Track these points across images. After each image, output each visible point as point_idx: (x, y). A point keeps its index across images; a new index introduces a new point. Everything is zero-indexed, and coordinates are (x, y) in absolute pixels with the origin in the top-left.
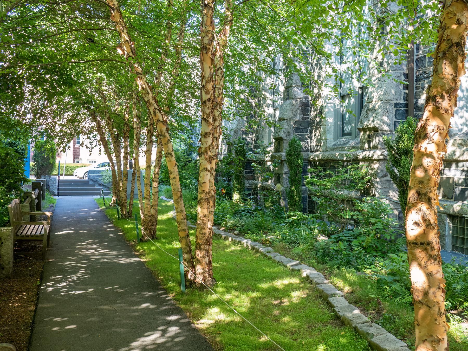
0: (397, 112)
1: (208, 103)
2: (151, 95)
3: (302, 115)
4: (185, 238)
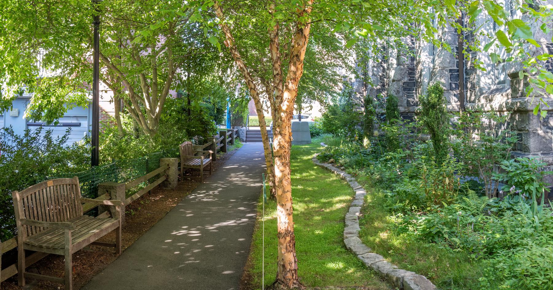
0: (452, 76)
1: (277, 76)
2: (246, 72)
3: (409, 78)
4: (270, 166)
